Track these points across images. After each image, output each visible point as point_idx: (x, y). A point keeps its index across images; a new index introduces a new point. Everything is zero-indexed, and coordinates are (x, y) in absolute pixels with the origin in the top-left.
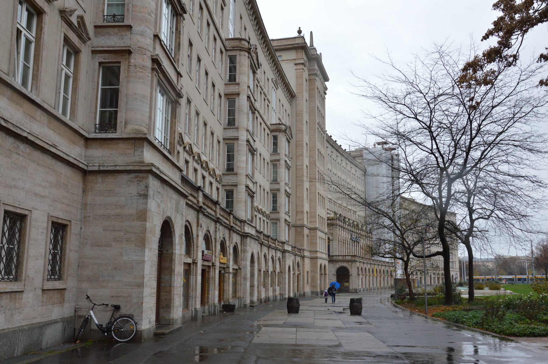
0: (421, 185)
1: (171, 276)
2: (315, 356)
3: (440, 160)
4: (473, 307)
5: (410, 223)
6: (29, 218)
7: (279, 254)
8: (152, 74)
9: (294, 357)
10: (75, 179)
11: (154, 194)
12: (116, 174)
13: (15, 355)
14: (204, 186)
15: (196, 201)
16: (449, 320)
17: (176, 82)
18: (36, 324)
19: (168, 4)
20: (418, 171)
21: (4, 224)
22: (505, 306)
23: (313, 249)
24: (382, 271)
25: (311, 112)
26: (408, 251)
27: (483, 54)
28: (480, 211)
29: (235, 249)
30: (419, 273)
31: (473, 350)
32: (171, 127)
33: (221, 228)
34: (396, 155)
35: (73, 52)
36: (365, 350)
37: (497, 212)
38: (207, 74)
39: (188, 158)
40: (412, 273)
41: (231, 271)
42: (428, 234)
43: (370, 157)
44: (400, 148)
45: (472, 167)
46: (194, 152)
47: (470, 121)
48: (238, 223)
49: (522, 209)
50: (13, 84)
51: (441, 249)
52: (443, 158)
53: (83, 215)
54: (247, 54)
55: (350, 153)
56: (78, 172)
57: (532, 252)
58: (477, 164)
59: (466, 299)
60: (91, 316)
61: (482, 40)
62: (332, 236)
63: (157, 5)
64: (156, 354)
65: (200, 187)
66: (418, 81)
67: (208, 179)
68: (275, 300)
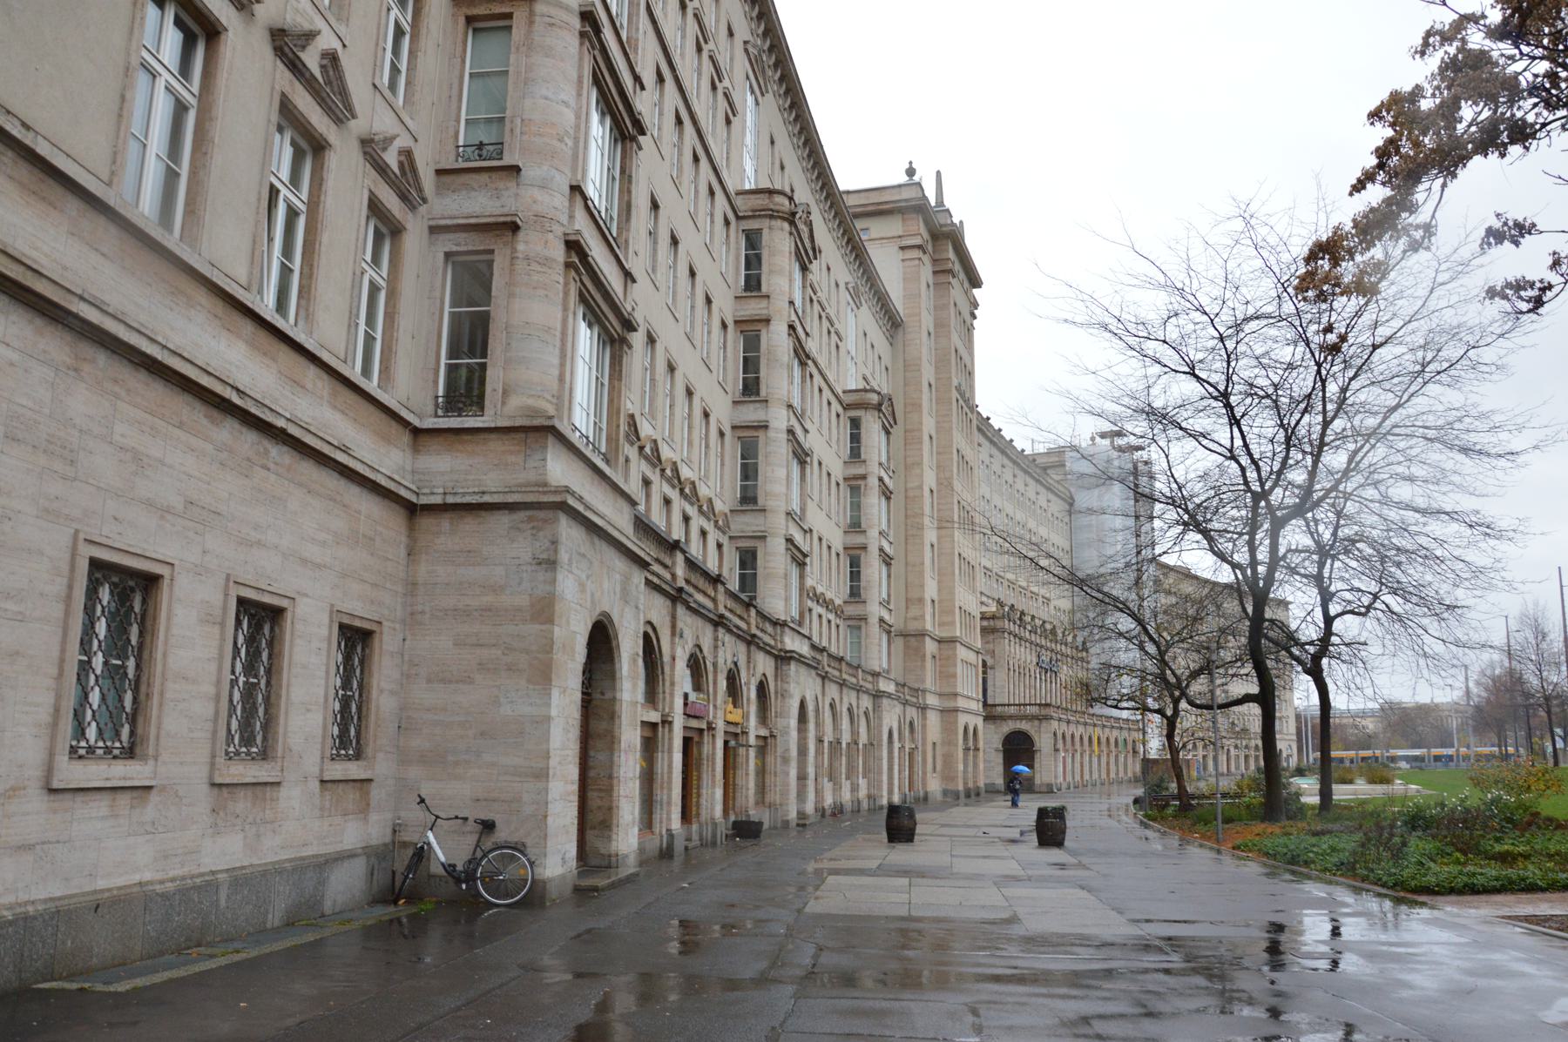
0: (1206, 533)
1: (612, 754)
3: (1252, 475)
4: (1330, 826)
6: (289, 615)
7: (866, 702)
8: (566, 277)
9: (904, 947)
10: (389, 522)
11: (570, 559)
12: (483, 513)
13: (269, 925)
15: (668, 576)
16: (1274, 857)
17: (621, 295)
19: (603, 114)
20: (1197, 501)
22: (1405, 823)
23: (948, 690)
24: (1112, 741)
25: (941, 363)
26: (1177, 693)
27: (1354, 220)
28: (1348, 596)
29: (762, 688)
30: (1200, 745)
31: (1329, 927)
32: (611, 401)
33: (728, 638)
34: (1146, 463)
35: (387, 229)
37: (1389, 599)
38: (693, 274)
39: (649, 474)
40: (1184, 746)
41: (752, 740)
43: (1085, 467)
44: (1154, 447)
45: (1329, 491)
46: (663, 458)
48: (769, 629)
49: (1444, 590)
52: (1258, 469)
54: (786, 225)
55: (1033, 459)
57: (1468, 692)
58: (1339, 482)
59: (1313, 807)
60: (429, 844)
61: (1351, 194)
62: (993, 657)
63: (578, 117)
64: (579, 936)
65: (677, 542)
66: (1195, 285)
67: (697, 522)
68: (857, 810)
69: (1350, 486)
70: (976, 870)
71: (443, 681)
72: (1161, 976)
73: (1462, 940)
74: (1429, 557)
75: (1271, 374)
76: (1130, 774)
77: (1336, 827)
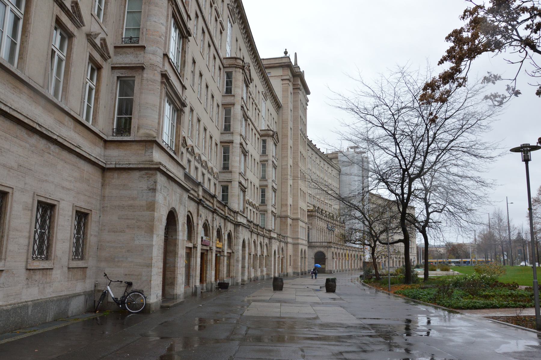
0: (387, 183)
2: (297, 327)
3: (403, 163)
4: (427, 286)
5: (376, 215)
6: (57, 207)
7: (266, 241)
9: (278, 328)
12: (130, 171)
14: (204, 182)
15: (196, 195)
18: (63, 296)
19: (176, 28)
20: (384, 171)
21: (37, 212)
22: (453, 285)
23: (295, 237)
24: (353, 255)
25: (295, 120)
26: (375, 239)
27: (439, 76)
29: (229, 235)
30: (383, 257)
32: (177, 132)
33: (217, 217)
34: (366, 158)
35: (96, 68)
36: (338, 322)
37: (449, 207)
38: (207, 87)
39: (190, 158)
40: (378, 257)
41: (226, 254)
42: (391, 225)
43: (344, 159)
44: (369, 152)
45: (429, 169)
46: (195, 153)
47: (427, 130)
48: (232, 214)
50: (47, 95)
51: (402, 238)
52: (405, 161)
53: (102, 206)
54: (241, 70)
55: (327, 156)
56: (98, 168)
57: (475, 239)
58: (433, 166)
59: (422, 279)
60: (108, 291)
61: (438, 65)
62: (312, 225)
63: (167, 29)
65: (200, 183)
66: (384, 96)
67: (207, 175)
68: (263, 279)
69: (436, 167)
70: (304, 301)
71: (114, 232)
72: (368, 338)
73: (471, 325)
74: (463, 193)
75: (410, 128)
76: (359, 267)
77: (429, 286)
